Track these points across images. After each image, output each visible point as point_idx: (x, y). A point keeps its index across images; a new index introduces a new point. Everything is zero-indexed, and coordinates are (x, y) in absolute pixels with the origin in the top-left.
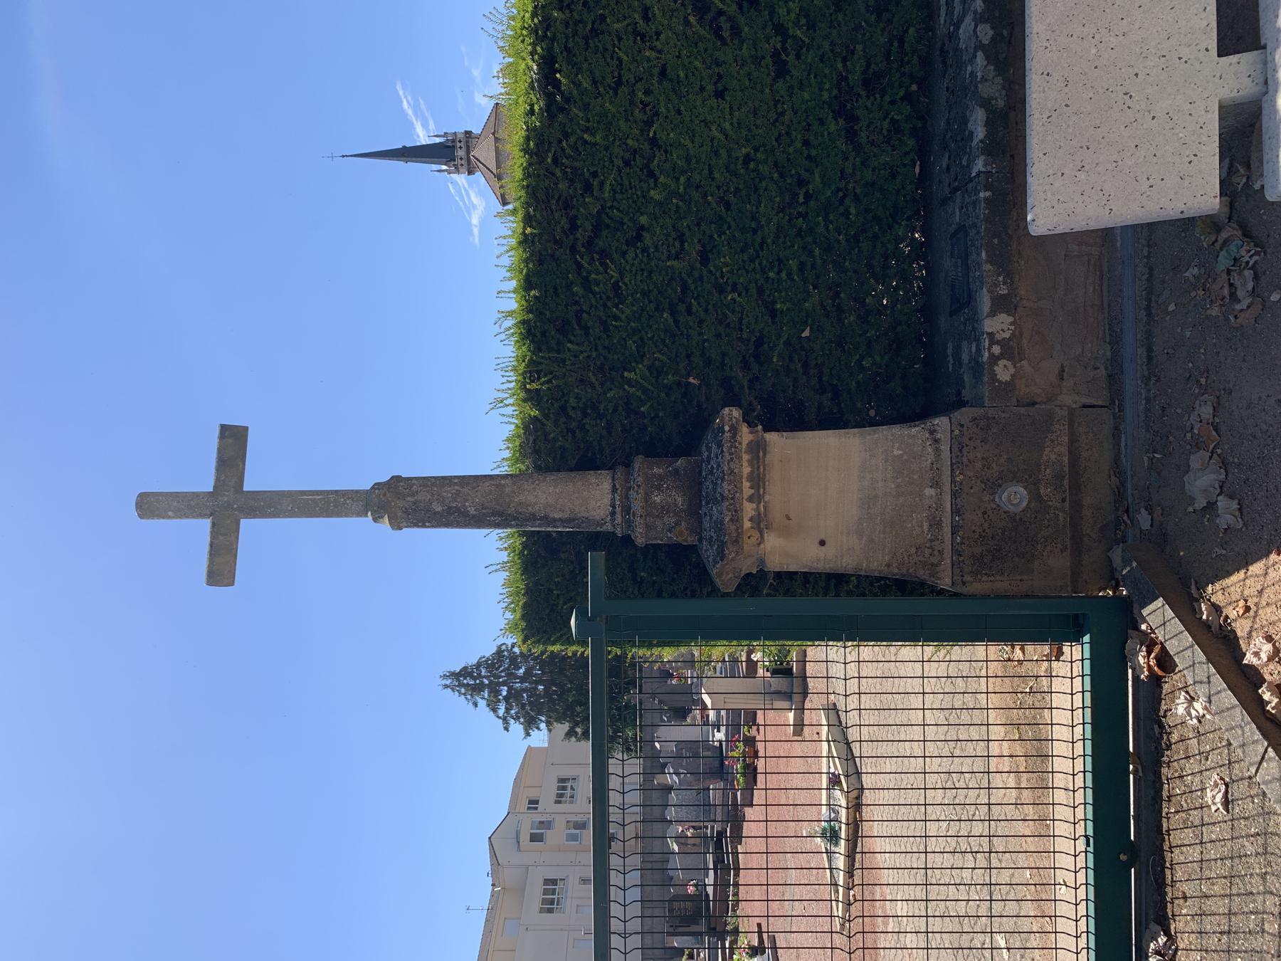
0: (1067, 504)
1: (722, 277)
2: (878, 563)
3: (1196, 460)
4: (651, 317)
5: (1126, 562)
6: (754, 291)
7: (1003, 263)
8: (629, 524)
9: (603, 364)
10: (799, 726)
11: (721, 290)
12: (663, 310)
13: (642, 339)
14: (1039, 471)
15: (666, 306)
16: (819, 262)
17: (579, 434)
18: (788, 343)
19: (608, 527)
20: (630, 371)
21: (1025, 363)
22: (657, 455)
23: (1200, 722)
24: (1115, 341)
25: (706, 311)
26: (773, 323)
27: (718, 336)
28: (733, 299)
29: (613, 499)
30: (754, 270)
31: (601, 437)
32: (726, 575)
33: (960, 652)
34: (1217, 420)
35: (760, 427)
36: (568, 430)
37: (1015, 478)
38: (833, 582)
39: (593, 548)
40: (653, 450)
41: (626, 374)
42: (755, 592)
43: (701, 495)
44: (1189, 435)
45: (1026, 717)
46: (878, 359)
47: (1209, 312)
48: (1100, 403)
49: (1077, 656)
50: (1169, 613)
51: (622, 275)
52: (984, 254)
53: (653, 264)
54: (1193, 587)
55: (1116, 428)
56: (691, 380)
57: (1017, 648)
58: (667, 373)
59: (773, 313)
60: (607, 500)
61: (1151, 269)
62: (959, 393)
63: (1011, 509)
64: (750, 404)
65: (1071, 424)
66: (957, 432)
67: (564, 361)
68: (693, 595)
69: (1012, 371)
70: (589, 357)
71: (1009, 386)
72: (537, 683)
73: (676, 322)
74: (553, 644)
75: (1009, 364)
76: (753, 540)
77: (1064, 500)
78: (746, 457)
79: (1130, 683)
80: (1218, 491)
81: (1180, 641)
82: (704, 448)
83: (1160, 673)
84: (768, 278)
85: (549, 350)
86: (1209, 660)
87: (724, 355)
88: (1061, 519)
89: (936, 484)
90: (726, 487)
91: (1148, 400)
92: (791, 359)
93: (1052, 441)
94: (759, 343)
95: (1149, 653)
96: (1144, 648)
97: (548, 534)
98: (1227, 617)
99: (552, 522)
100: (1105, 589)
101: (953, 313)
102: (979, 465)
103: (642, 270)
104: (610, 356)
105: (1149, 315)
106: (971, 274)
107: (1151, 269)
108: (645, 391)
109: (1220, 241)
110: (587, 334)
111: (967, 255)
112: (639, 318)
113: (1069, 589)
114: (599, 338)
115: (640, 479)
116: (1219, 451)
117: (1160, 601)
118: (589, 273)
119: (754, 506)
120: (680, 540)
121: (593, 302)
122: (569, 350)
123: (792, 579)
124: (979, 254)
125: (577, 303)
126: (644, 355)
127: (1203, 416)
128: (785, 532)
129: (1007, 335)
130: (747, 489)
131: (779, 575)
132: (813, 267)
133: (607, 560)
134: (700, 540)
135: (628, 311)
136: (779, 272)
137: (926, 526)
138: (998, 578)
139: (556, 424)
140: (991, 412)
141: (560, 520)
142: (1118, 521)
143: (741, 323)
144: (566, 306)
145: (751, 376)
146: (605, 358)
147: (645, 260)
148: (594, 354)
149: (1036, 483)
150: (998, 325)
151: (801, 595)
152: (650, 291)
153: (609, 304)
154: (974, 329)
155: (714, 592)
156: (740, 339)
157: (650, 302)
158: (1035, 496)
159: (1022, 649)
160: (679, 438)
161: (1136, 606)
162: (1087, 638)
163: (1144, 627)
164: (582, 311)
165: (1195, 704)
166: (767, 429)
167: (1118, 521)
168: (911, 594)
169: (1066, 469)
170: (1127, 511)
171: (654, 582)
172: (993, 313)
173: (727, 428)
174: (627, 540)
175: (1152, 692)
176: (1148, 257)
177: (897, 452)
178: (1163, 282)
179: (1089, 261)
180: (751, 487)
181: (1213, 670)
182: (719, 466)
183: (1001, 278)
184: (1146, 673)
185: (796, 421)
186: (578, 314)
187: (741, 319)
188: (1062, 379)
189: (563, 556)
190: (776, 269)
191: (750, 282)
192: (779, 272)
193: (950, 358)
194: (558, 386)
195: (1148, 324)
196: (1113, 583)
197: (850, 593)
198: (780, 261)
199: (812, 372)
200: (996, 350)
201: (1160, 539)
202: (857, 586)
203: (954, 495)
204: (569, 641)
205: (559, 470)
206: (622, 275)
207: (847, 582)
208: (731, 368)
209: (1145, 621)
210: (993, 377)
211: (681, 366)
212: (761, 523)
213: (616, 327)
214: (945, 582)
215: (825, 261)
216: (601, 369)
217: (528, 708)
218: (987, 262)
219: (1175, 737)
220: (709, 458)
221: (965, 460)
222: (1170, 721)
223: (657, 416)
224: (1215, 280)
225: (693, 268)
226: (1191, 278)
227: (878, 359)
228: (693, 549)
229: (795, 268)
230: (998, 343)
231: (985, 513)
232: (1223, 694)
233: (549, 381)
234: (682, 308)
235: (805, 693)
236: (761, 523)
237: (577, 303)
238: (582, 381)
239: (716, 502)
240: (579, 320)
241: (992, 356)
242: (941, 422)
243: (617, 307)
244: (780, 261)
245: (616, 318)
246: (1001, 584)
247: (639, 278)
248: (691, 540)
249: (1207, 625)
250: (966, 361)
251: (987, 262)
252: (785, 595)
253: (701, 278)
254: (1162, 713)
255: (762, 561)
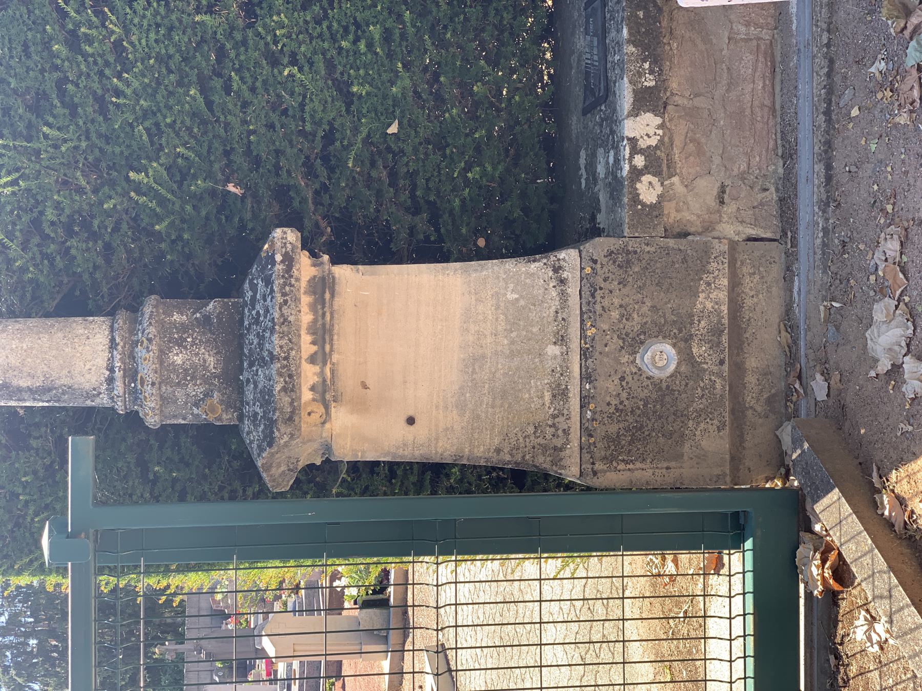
0: (726, 367)
1: (276, 43)
2: (482, 446)
3: (880, 311)
4: (171, 94)
5: (796, 443)
6: (321, 66)
7: (651, 44)
8: (135, 395)
9: (98, 160)
10: (397, 673)
11: (274, 62)
12: (190, 84)
13: (157, 125)
14: (692, 323)
15: (195, 79)
16: (411, 30)
17: (59, 262)
18: (367, 141)
19: (104, 401)
20: (138, 171)
21: (675, 179)
22: (183, 296)
23: (882, 648)
24: (789, 155)
25: (253, 90)
26: (348, 111)
27: (271, 126)
28: (291, 75)
29: (111, 359)
30: (320, 36)
31: (96, 267)
32: (279, 465)
33: (600, 565)
34: (905, 259)
35: (326, 257)
36: (45, 256)
37: (660, 331)
38: (428, 475)
39: (80, 430)
40: (178, 287)
41: (131, 174)
42: (322, 491)
43: (243, 353)
44: (872, 278)
45: (680, 652)
46: (489, 168)
47: (897, 119)
48: (768, 235)
49: (737, 566)
50: (847, 509)
51: (127, 31)
52: (625, 31)
53: (174, 17)
54: (875, 474)
55: (788, 269)
56: (231, 188)
57: (669, 558)
58: (195, 177)
59: (349, 99)
60: (101, 360)
61: (831, 62)
62: (593, 218)
63: (656, 373)
64: (317, 225)
65: (732, 263)
66: (588, 270)
67: (38, 153)
68: (233, 498)
69: (659, 189)
70: (76, 148)
71: (656, 209)
72: (27, 635)
73: (209, 104)
74: (19, 573)
75: (655, 180)
76: (315, 417)
77: (722, 362)
78: (306, 300)
79: (802, 602)
80: (904, 351)
81: (858, 544)
82: (247, 286)
83: (836, 587)
84: (340, 48)
85: (15, 136)
86: (891, 568)
87: (278, 153)
88: (718, 386)
89: (561, 340)
90: (276, 343)
91: (825, 230)
92: (373, 164)
93: (709, 284)
94: (329, 138)
95: (824, 561)
96: (818, 556)
97: (12, 411)
98: (912, 512)
99: (18, 392)
100: (772, 479)
101: (585, 112)
102: (615, 314)
103: (158, 25)
104: (109, 149)
105: (829, 121)
106: (610, 59)
107: (831, 62)
108: (162, 202)
109: (910, 28)
110: (74, 114)
111: (605, 32)
112: (153, 95)
113: (728, 479)
114: (93, 121)
115: (152, 330)
116: (907, 299)
117: (835, 494)
118: (78, 25)
119: (317, 369)
120: (211, 418)
121: (83, 67)
122: (46, 136)
123: (372, 472)
124: (619, 31)
125: (56, 68)
126: (161, 148)
127: (889, 253)
128: (360, 406)
129: (653, 142)
130: (307, 345)
131: (355, 467)
132: (403, 36)
133: (97, 448)
134: (241, 418)
135: (136, 84)
136: (356, 41)
137: (547, 396)
138: (639, 465)
139: (25, 247)
140: (632, 245)
141: (29, 389)
142: (789, 391)
143: (303, 111)
144: (43, 71)
145: (317, 186)
146: (101, 150)
147: (162, 10)
148: (84, 144)
149: (688, 339)
150: (642, 128)
151: (385, 494)
152: (170, 57)
153: (107, 72)
154: (613, 132)
155: (262, 492)
156: (302, 133)
157: (170, 71)
158: (686, 357)
159: (675, 561)
160: (212, 271)
161: (808, 500)
162: (749, 544)
163: (817, 528)
164: (66, 80)
165: (876, 625)
166: (336, 260)
167: (789, 391)
168: (531, 489)
169: (725, 321)
170: (800, 377)
171: (175, 481)
172: (635, 112)
173: (278, 258)
174: (134, 419)
175: (828, 609)
176: (828, 45)
177: (512, 296)
178: (845, 78)
179: (758, 46)
180: (314, 343)
181: (895, 581)
182: (267, 311)
183: (647, 65)
184: (820, 588)
185: (379, 249)
186: (60, 84)
187: (302, 106)
188: (722, 202)
189: (34, 443)
190: (351, 37)
191: (315, 52)
192: (356, 41)
193: (583, 171)
194: (28, 190)
195: (827, 132)
196: (783, 471)
197: (451, 490)
198: (358, 26)
199: (401, 183)
200: (639, 161)
201: (838, 414)
202: (461, 481)
203: (585, 354)
204: (42, 570)
205: (28, 316)
206: (127, 31)
207: (448, 476)
208: (289, 172)
209: (819, 520)
210: (635, 198)
211: (216, 166)
212: (326, 393)
213: (117, 106)
214: (571, 473)
215: (418, 30)
216: (95, 166)
217: (13, 672)
218: (629, 41)
219: (853, 670)
220: (254, 298)
221: (598, 307)
222: (847, 649)
223: (180, 238)
224: (903, 78)
225: (232, 28)
226: (877, 74)
227: (489, 168)
228: (233, 431)
229: (377, 37)
230: (641, 152)
231: (622, 379)
232: (906, 611)
233: (14, 183)
234: (217, 83)
235: (405, 629)
236: (326, 393)
237: (56, 68)
238: (65, 183)
239: (264, 363)
240: (62, 93)
241: (633, 169)
242: (569, 256)
243: (119, 77)
244: (358, 26)
245: (118, 93)
246: (643, 473)
247: (152, 36)
248: (227, 418)
249: (889, 524)
250: (602, 176)
251: (629, 41)
252: (363, 494)
253: (244, 42)
254: (838, 640)
255: (328, 448)
